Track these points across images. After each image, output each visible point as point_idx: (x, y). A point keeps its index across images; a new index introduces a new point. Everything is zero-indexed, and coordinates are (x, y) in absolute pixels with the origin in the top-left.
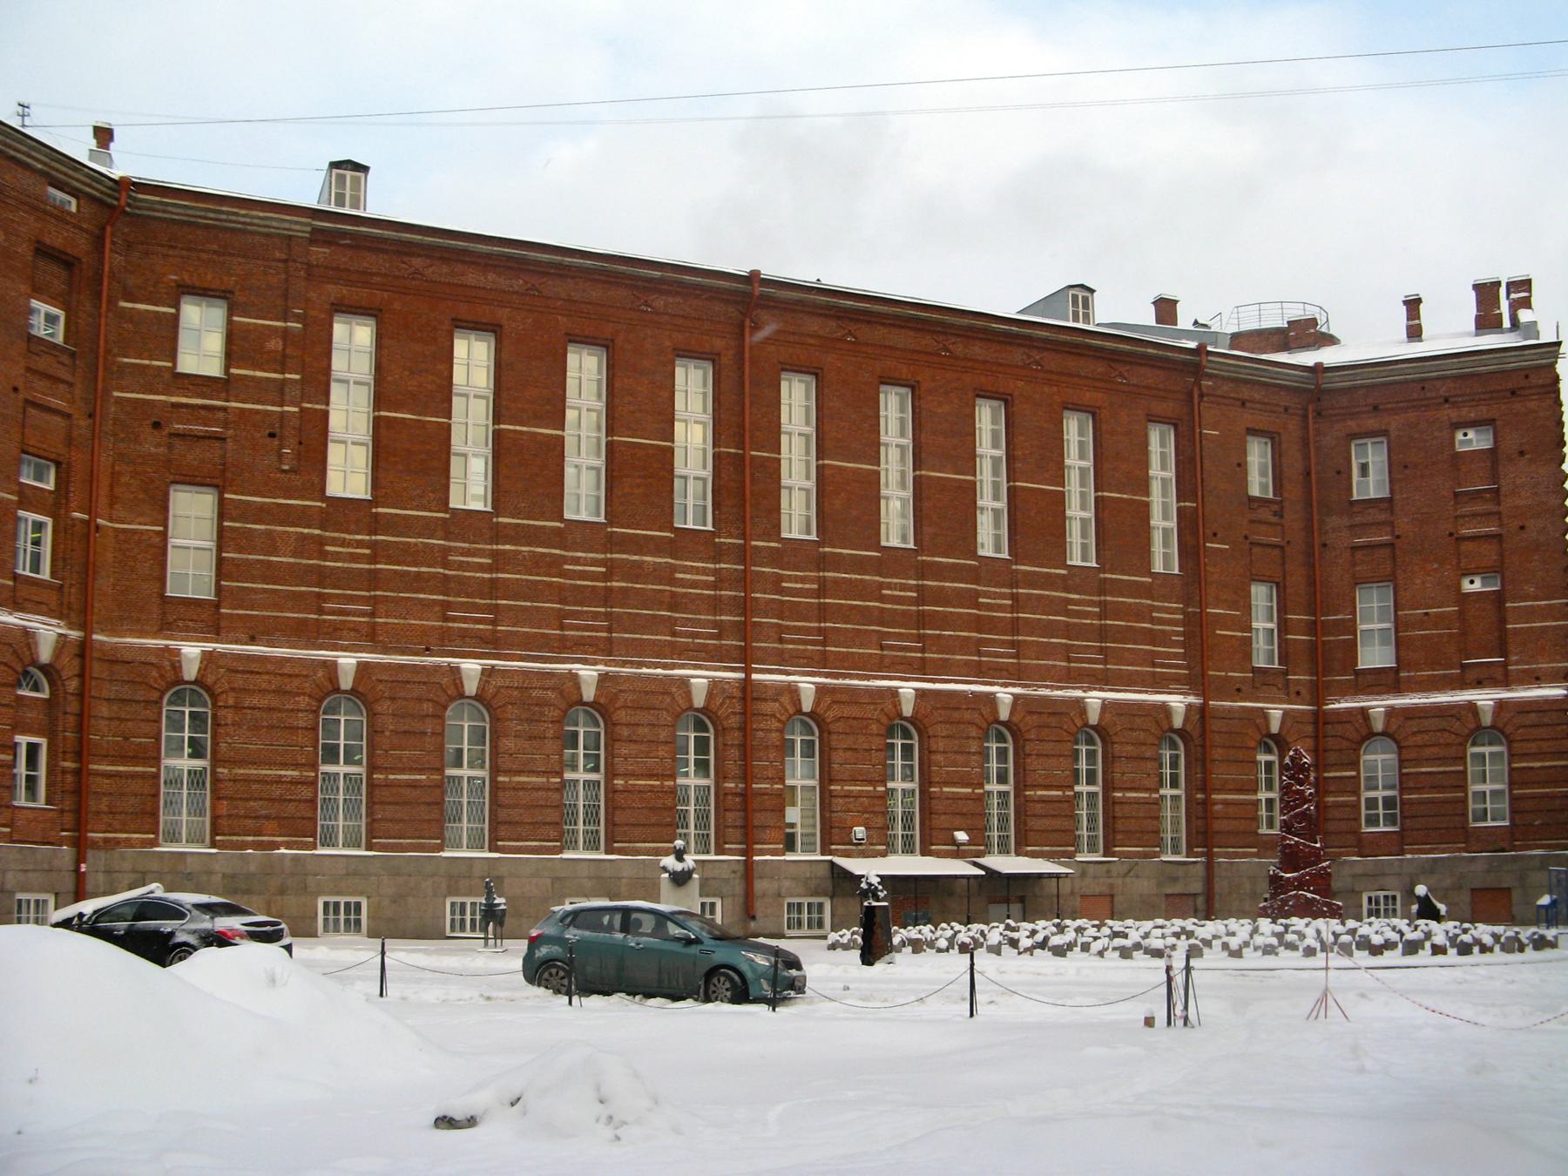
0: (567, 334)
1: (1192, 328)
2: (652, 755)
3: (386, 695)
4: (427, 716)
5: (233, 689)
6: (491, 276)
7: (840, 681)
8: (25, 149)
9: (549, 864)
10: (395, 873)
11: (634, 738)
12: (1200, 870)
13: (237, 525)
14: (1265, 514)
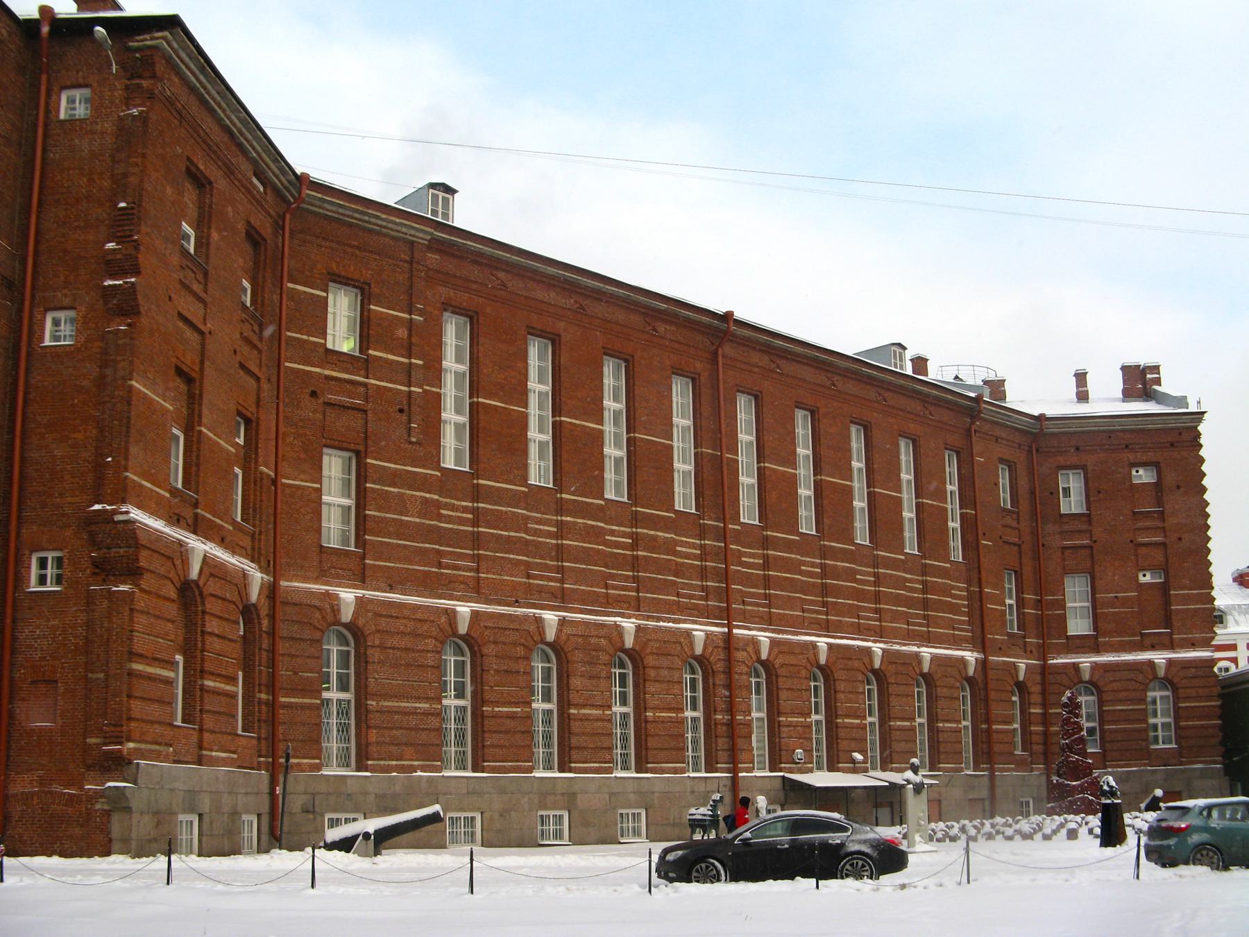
0: (604, 348)
1: (953, 381)
3: (491, 639)
4: (520, 658)
5: (378, 631)
6: (553, 294)
7: (780, 636)
10: (502, 791)
11: (658, 678)
12: (986, 781)
13: (377, 487)
14: (1009, 520)
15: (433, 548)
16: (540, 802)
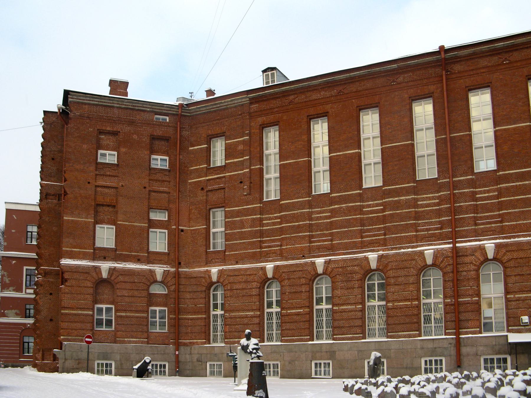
2: (406, 290)
3: (286, 278)
5: (230, 283)
8: (141, 105)
9: (356, 344)
10: (290, 351)
13: (230, 220)
15: (257, 240)
16: (312, 356)
